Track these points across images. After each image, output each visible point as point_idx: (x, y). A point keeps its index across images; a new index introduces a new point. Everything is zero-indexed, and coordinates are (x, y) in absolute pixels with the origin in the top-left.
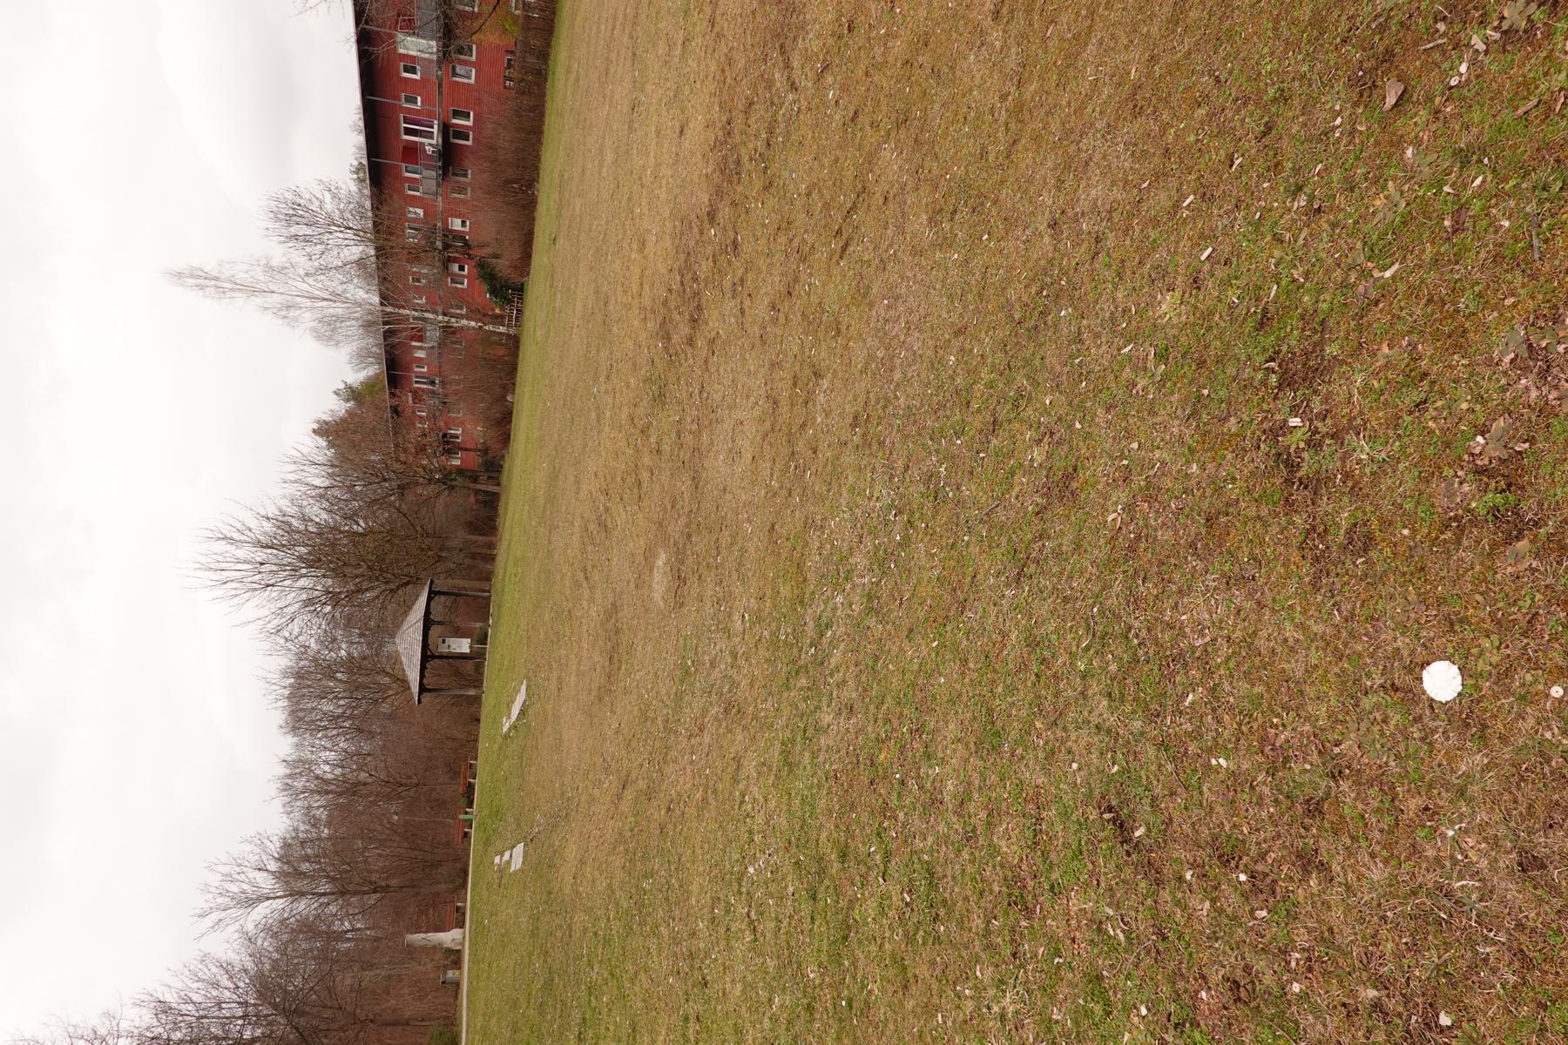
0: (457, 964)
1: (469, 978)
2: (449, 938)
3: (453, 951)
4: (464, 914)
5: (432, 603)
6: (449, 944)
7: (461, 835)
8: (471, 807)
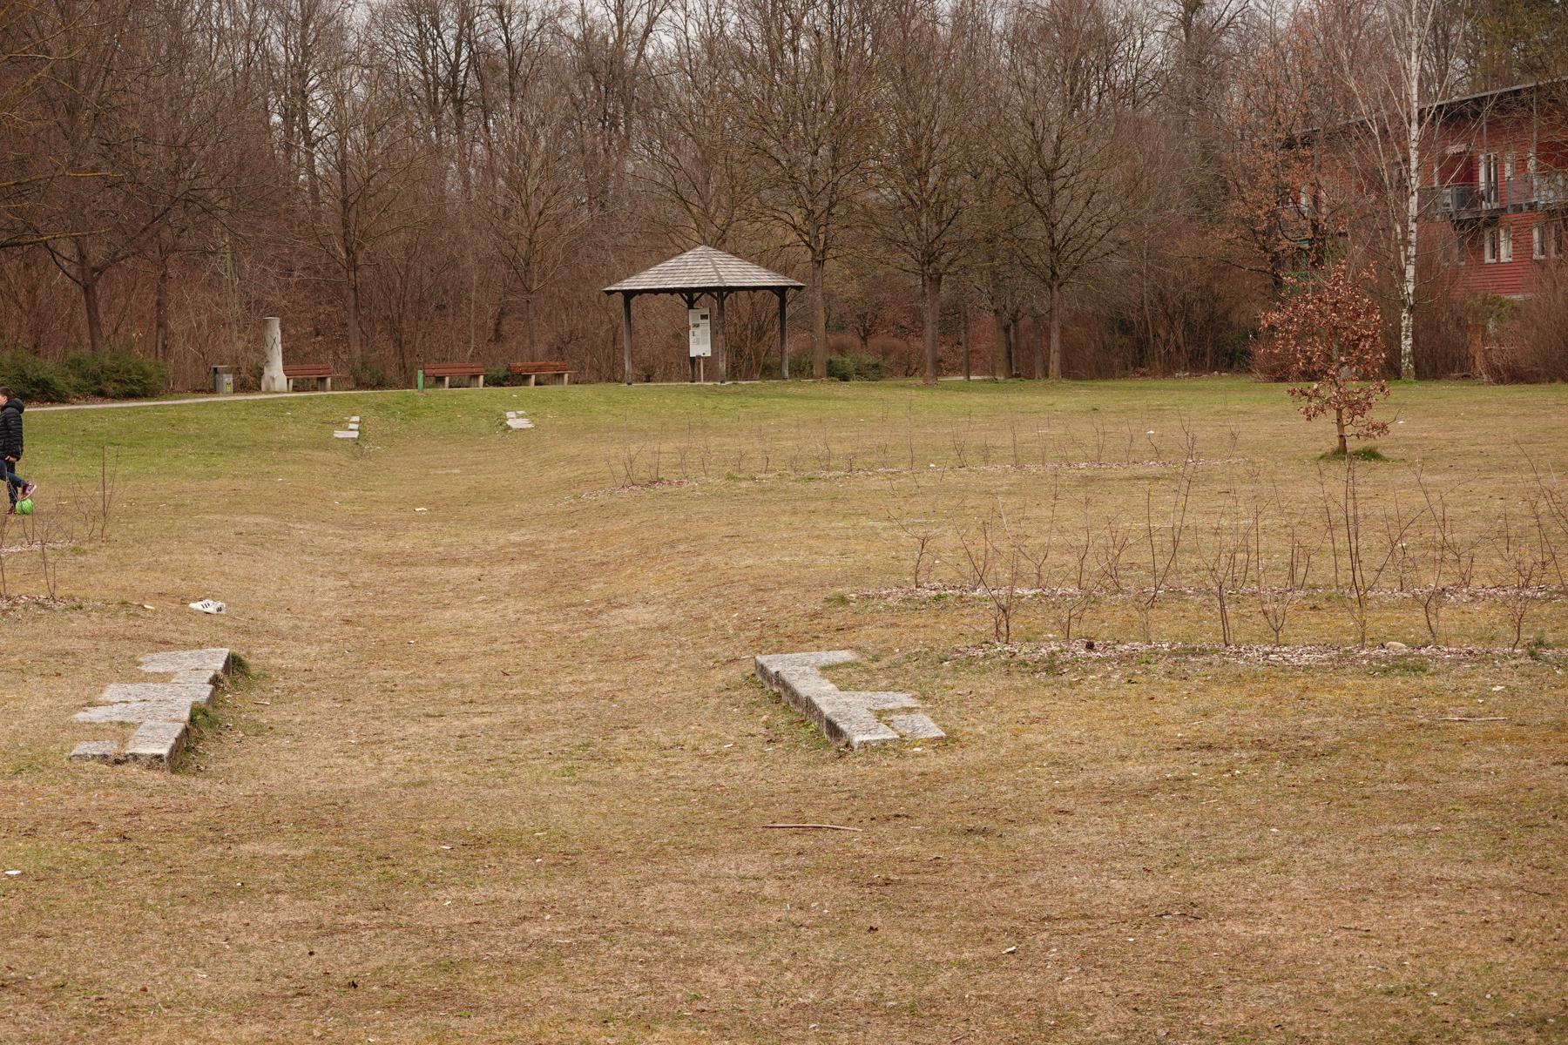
0: (242, 387)
1: (229, 402)
2: (276, 373)
3: (260, 379)
4: (315, 389)
5: (677, 297)
6: (267, 373)
7: (438, 373)
8: (486, 383)
